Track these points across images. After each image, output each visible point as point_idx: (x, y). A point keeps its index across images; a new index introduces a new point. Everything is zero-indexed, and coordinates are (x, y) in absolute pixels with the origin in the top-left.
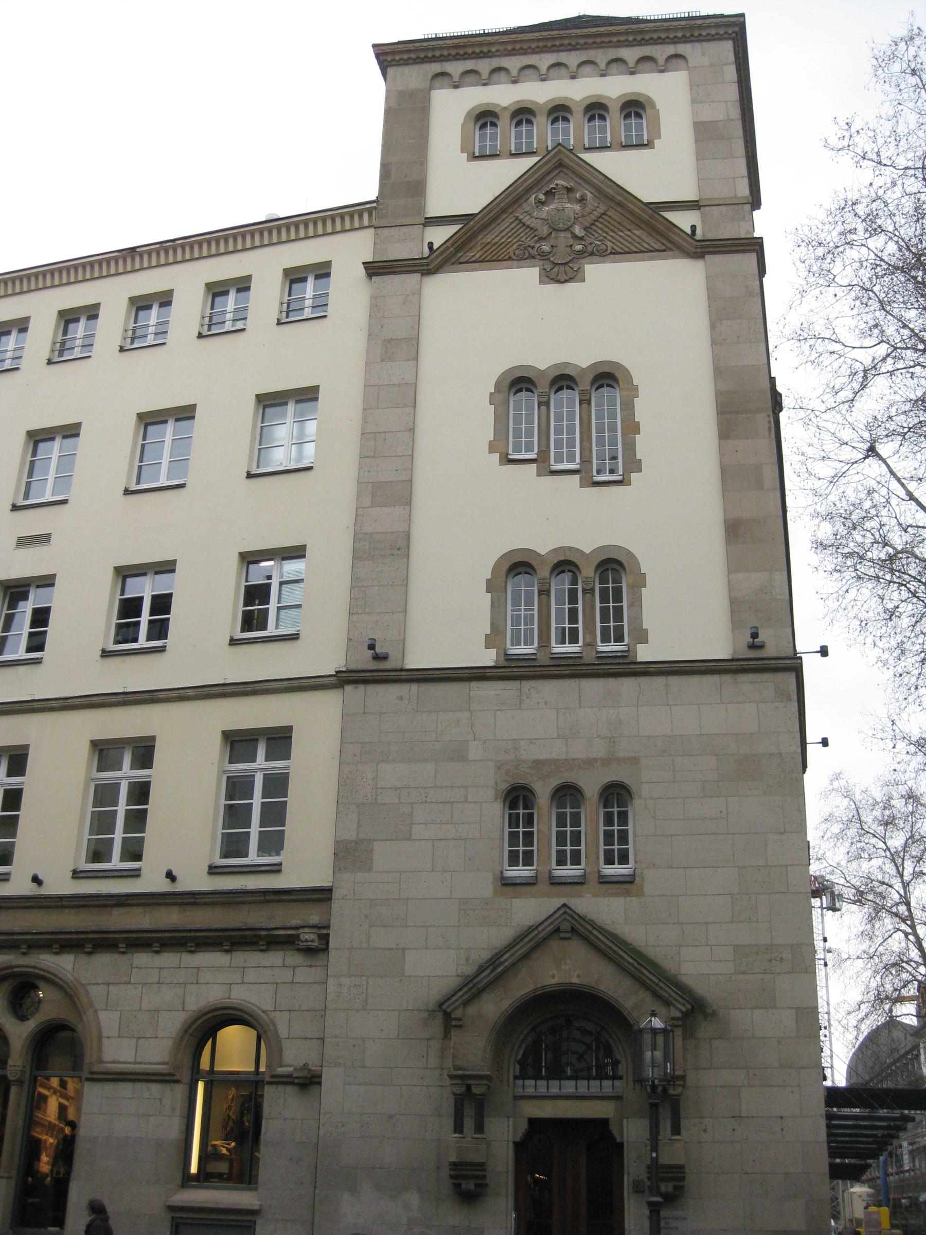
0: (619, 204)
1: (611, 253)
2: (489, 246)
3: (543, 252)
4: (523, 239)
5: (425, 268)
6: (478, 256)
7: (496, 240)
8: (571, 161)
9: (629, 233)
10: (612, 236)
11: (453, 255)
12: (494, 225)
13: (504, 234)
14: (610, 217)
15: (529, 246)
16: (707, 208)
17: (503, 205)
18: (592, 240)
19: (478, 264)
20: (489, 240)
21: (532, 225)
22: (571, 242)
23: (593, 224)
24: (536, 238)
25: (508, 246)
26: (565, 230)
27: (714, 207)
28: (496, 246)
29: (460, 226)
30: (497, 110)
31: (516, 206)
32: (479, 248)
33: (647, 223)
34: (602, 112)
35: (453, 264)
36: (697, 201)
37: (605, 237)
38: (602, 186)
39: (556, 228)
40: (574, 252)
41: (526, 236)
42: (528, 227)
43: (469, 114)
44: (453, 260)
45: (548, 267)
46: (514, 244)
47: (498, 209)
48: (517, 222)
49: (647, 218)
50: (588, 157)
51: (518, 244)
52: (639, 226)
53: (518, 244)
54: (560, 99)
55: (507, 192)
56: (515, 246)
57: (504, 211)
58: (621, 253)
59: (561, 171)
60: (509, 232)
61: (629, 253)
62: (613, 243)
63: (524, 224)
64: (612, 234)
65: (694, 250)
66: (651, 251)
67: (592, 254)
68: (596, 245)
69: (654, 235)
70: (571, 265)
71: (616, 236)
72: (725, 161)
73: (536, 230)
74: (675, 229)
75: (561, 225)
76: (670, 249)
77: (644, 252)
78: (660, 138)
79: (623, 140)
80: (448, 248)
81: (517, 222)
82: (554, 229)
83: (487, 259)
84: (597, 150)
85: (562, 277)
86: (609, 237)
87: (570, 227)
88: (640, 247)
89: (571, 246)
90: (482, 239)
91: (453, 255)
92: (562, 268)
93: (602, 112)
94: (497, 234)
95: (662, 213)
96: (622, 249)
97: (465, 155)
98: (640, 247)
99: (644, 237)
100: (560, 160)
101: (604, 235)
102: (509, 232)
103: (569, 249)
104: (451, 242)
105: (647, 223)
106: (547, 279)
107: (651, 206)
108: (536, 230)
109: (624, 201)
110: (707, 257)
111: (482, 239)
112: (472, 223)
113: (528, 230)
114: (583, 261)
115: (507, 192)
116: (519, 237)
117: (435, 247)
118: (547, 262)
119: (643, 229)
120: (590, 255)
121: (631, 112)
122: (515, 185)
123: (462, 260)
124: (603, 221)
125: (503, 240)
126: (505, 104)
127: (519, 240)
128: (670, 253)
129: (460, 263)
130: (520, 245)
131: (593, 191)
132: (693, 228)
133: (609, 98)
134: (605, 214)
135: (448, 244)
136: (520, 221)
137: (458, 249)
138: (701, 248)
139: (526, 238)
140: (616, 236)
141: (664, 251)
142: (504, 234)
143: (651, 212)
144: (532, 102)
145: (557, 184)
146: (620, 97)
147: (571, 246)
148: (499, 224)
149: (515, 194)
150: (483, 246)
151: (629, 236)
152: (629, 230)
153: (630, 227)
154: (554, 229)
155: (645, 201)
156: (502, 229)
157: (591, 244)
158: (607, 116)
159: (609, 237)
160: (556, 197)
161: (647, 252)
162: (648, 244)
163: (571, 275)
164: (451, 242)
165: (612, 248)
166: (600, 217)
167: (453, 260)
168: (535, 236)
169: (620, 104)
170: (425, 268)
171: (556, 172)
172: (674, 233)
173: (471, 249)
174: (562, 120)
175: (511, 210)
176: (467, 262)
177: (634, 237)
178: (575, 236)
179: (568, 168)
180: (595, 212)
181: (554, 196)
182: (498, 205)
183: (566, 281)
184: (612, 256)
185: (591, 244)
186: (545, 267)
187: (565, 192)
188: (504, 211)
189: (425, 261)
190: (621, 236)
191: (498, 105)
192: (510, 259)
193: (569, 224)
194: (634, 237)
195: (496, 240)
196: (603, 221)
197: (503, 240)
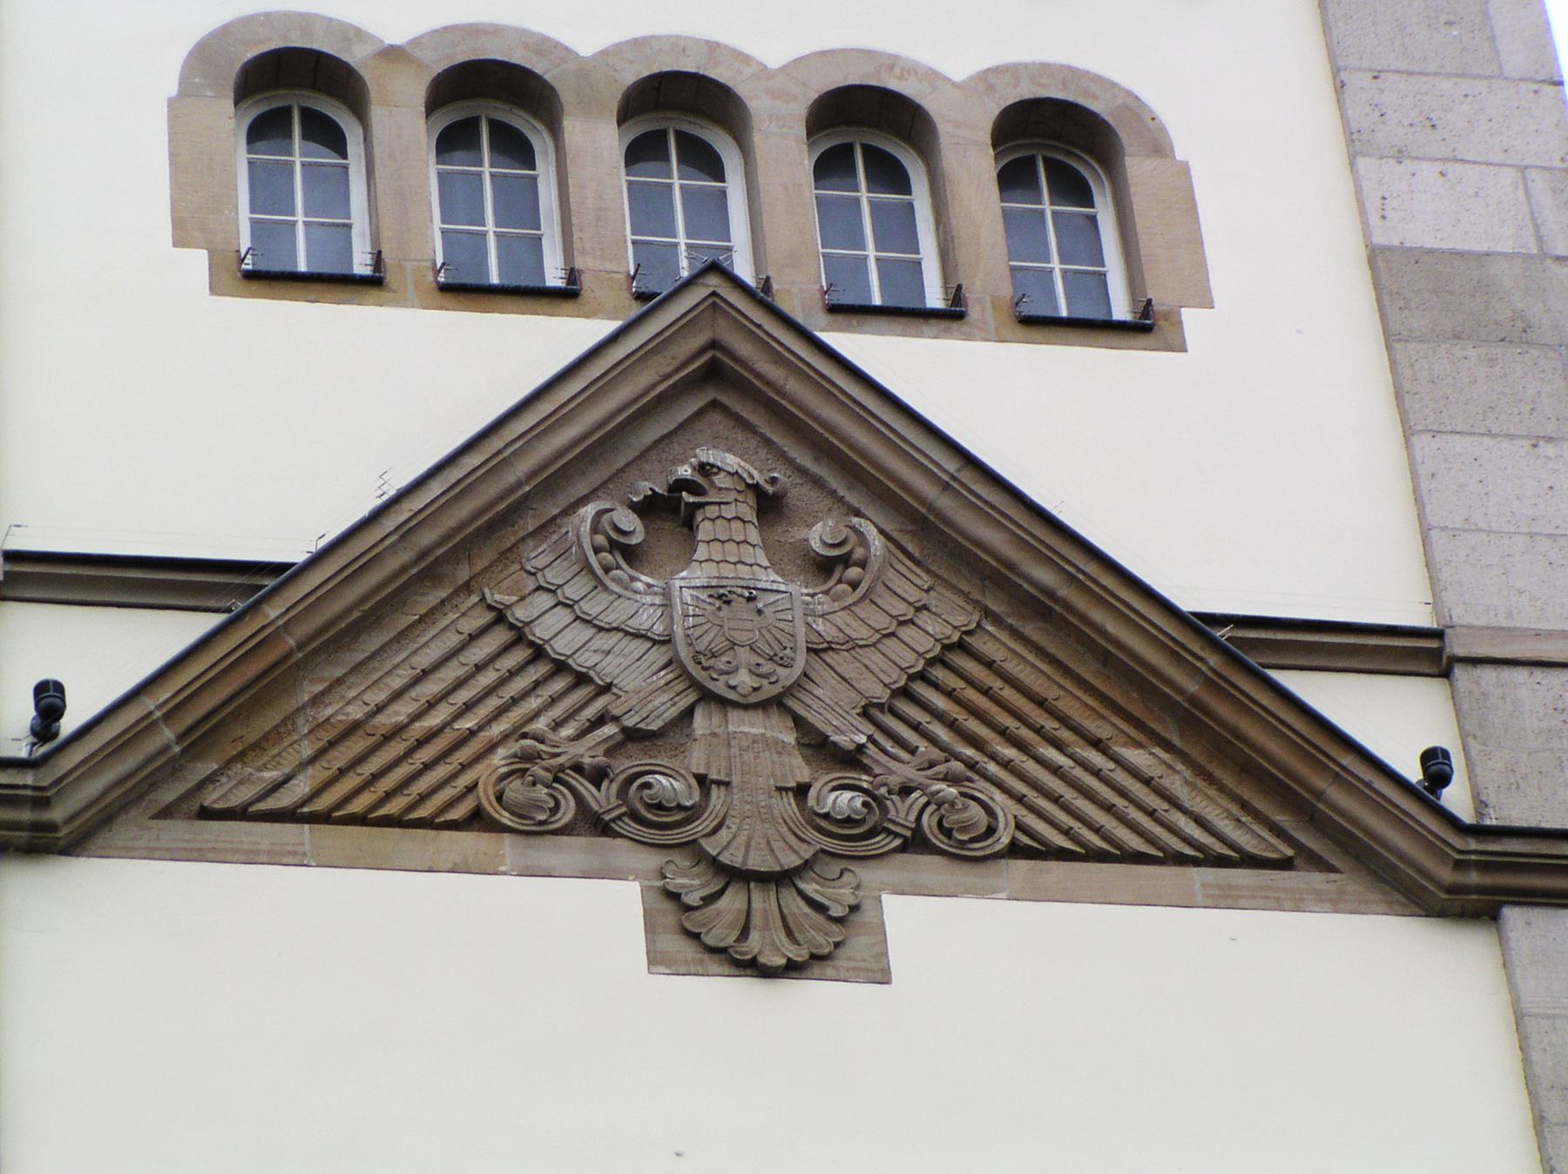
0: (1041, 607)
1: (1015, 851)
2: (357, 745)
3: (659, 807)
4: (541, 725)
5: (26, 815)
6: (301, 787)
7: (400, 712)
8: (779, 360)
9: (1096, 758)
10: (1006, 765)
11: (171, 767)
12: (372, 643)
13: (430, 688)
14: (989, 665)
15: (578, 768)
16: (1488, 675)
17: (426, 538)
18: (906, 771)
19: (302, 834)
20: (356, 712)
21: (583, 661)
22: (799, 769)
23: (905, 693)
24: (609, 730)
25: (463, 755)
26: (764, 705)
27: (1521, 674)
28: (396, 749)
29: (211, 621)
30: (355, 56)
31: (490, 554)
32: (307, 751)
33: (1192, 718)
34: (519, 120)
35: (166, 813)
36: (1437, 634)
37: (972, 765)
38: (945, 503)
39: (719, 688)
40: (823, 822)
41: (557, 712)
42: (560, 667)
43: (203, 55)
44: (168, 794)
45: (693, 885)
46: (491, 748)
47: (405, 556)
48: (500, 637)
49: (1192, 687)
50: (851, 343)
51: (515, 747)
52: (1139, 724)
53: (515, 747)
54: (1070, 74)
55: (455, 474)
56: (499, 758)
57: (429, 571)
58: (1062, 855)
59: (714, 405)
60: (460, 684)
61: (1101, 857)
62: (1020, 799)
63: (539, 653)
64: (1010, 752)
65: (1447, 875)
66: (1221, 862)
67: (916, 843)
68: (934, 800)
69: (1228, 780)
70: (810, 888)
71: (1031, 767)
72: (1549, 450)
73: (606, 689)
74: (1348, 760)
75: (744, 679)
76: (1317, 863)
77: (1180, 860)
78: (1205, 300)
79: (245, 242)
80: (146, 727)
81: (500, 637)
82: (708, 697)
83: (357, 806)
84: (1061, 333)
85: (767, 945)
86: (992, 768)
87: (789, 691)
88: (1123, 834)
89: (801, 791)
90: (316, 700)
91: (171, 767)
92: (763, 901)
93: (519, 120)
94: (396, 683)
95: (1291, 681)
96: (1067, 832)
97: (198, 259)
98: (1123, 834)
99: (1176, 784)
100: (714, 344)
101: (970, 752)
102: (460, 684)
103: (789, 805)
104: (164, 693)
105: (1192, 718)
106: (688, 950)
107: (1222, 633)
108: (606, 689)
109: (1064, 592)
110: (1513, 916)
111: (316, 700)
112: (272, 611)
113: (559, 684)
114: (868, 875)
115: (455, 474)
116: (515, 715)
117: (69, 724)
118: (682, 860)
119: (1167, 746)
120: (903, 849)
121: (1031, 161)
122: (496, 443)
123: (213, 798)
124: (953, 682)
125: (434, 720)
126: (396, 34)
127: (518, 732)
128: (1317, 879)
129: (207, 814)
130: (529, 757)
131: (887, 527)
132: (1436, 765)
133: (933, 77)
134: (961, 646)
135: (149, 703)
136: (520, 637)
137: (198, 740)
138: (1484, 868)
139: (557, 725)
140: (1031, 767)
141: (1285, 864)
142: (430, 688)
143: (1214, 660)
144: (545, 46)
145: (704, 469)
146: (988, 78)
147: (801, 791)
148: (403, 634)
149: (491, 490)
150: (327, 736)
151: (1097, 773)
152: (1097, 744)
153: (1102, 731)
154: (708, 697)
155: (1188, 603)
156: (424, 660)
157: (905, 791)
158: (541, 143)
159: (992, 768)
160: (705, 530)
161: (1195, 862)
162: (1200, 821)
163: (818, 935)
164: (164, 693)
165: (1020, 826)
166: (939, 661)
167: (168, 794)
168: (600, 720)
169: (995, 112)
170: (26, 815)
171: (691, 405)
172: (1340, 778)
173: (258, 746)
174: (306, 136)
175: (464, 574)
176: (241, 814)
177: (1121, 777)
178: (818, 746)
179: (743, 387)
180: (907, 633)
181: (689, 525)
182: (406, 532)
183: (792, 969)
184: (1021, 866)
185: (905, 791)
186: (677, 882)
187: (747, 511)
188: (429, 571)
189: (29, 778)
190: (1056, 770)
191: (360, 34)
192: (478, 820)
193: (787, 676)
194: (1121, 777)
195: (400, 712)
196: (953, 682)
197: (434, 720)
